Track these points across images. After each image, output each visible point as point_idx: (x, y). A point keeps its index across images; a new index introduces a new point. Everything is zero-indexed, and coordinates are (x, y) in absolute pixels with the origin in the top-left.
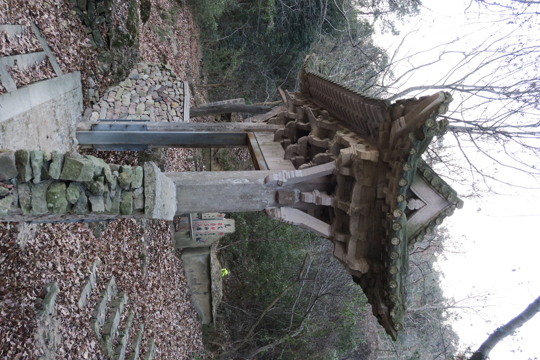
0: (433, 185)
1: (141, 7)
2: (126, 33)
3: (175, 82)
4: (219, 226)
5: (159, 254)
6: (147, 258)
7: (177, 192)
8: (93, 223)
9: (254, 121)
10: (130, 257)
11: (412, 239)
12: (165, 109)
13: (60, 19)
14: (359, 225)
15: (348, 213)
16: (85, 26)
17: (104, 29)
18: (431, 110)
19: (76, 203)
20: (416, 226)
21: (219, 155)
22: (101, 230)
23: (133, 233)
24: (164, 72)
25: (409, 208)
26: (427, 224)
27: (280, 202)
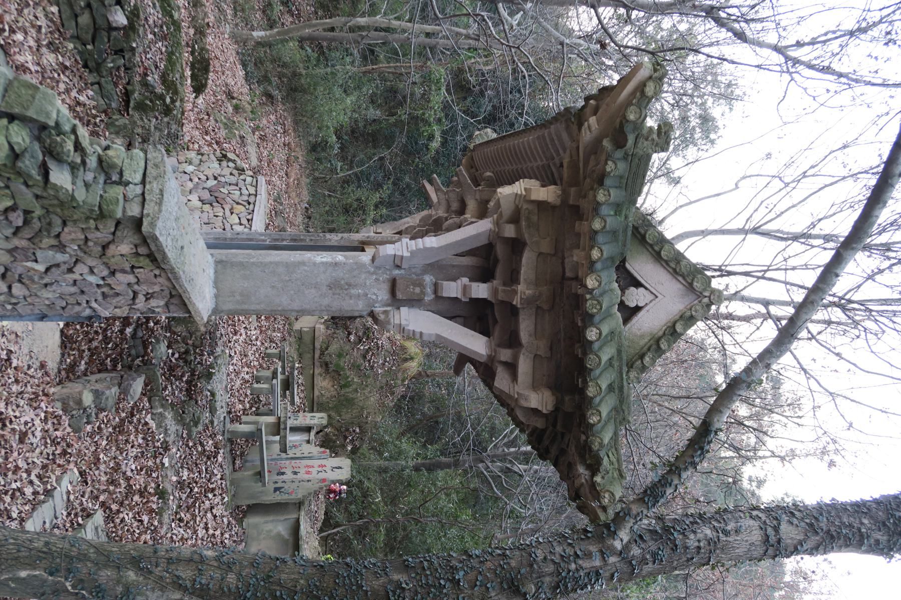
0: (665, 258)
1: (193, 68)
2: (160, 91)
3: (242, 177)
4: (320, 469)
5: (197, 499)
6: (172, 498)
7: (216, 272)
8: (71, 403)
9: (379, 231)
10: (138, 487)
11: (636, 361)
12: (221, 214)
13: (44, 50)
14: (536, 328)
15: (514, 303)
16: (87, 70)
17: (121, 78)
18: (633, 94)
19: (23, 152)
20: (642, 336)
21: (330, 356)
22: (85, 420)
23: (147, 445)
24: (224, 163)
25: (627, 303)
26: (661, 333)
27: (400, 295)
